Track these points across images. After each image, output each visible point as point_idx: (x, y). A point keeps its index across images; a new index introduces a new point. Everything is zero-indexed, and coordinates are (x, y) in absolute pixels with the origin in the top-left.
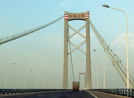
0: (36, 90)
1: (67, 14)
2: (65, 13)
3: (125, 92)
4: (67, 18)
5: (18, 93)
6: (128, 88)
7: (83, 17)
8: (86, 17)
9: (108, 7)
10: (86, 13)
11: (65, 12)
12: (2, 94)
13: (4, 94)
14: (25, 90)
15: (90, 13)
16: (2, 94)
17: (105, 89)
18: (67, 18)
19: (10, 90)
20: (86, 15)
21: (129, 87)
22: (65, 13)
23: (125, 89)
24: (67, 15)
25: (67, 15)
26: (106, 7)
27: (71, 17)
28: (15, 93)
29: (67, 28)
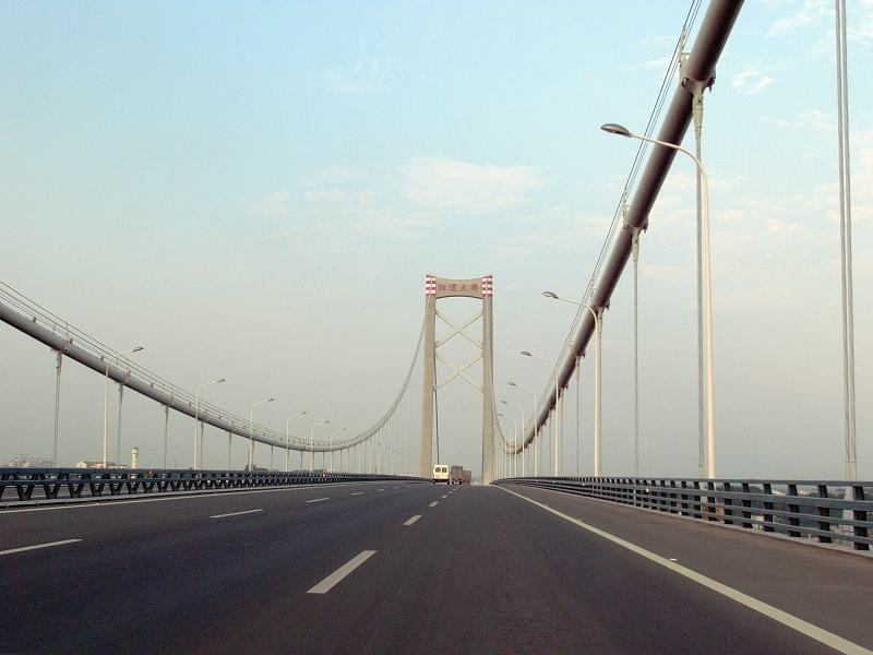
0: (231, 475)
1: (434, 282)
2: (428, 279)
3: (704, 494)
4: (434, 292)
5: (132, 490)
6: (596, 475)
7: (478, 289)
8: (484, 292)
9: (623, 132)
10: (484, 280)
11: (428, 276)
12: (10, 493)
13: (25, 494)
14: (194, 475)
15: (493, 280)
16: (10, 493)
17: (558, 479)
18: (434, 292)
19: (38, 474)
20: (484, 286)
21: (561, 465)
22: (428, 279)
23: (678, 480)
24: (434, 286)
25: (434, 286)
26: (617, 132)
27: (443, 289)
28: (96, 492)
29: (432, 313)
